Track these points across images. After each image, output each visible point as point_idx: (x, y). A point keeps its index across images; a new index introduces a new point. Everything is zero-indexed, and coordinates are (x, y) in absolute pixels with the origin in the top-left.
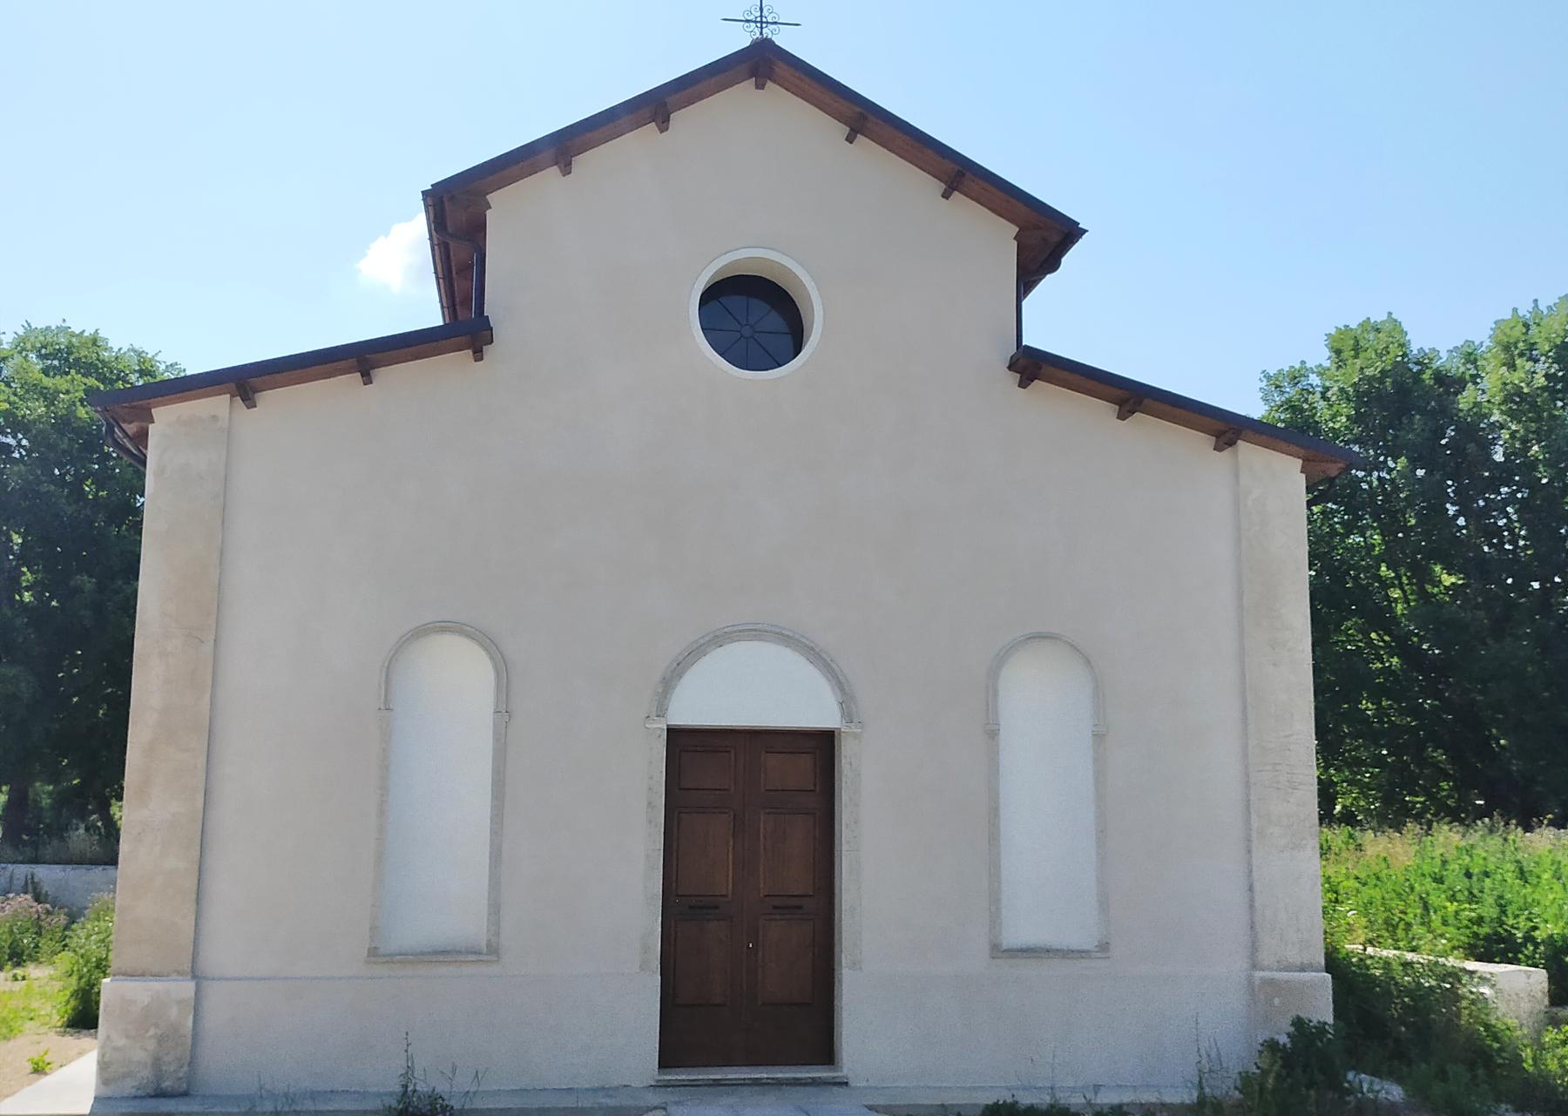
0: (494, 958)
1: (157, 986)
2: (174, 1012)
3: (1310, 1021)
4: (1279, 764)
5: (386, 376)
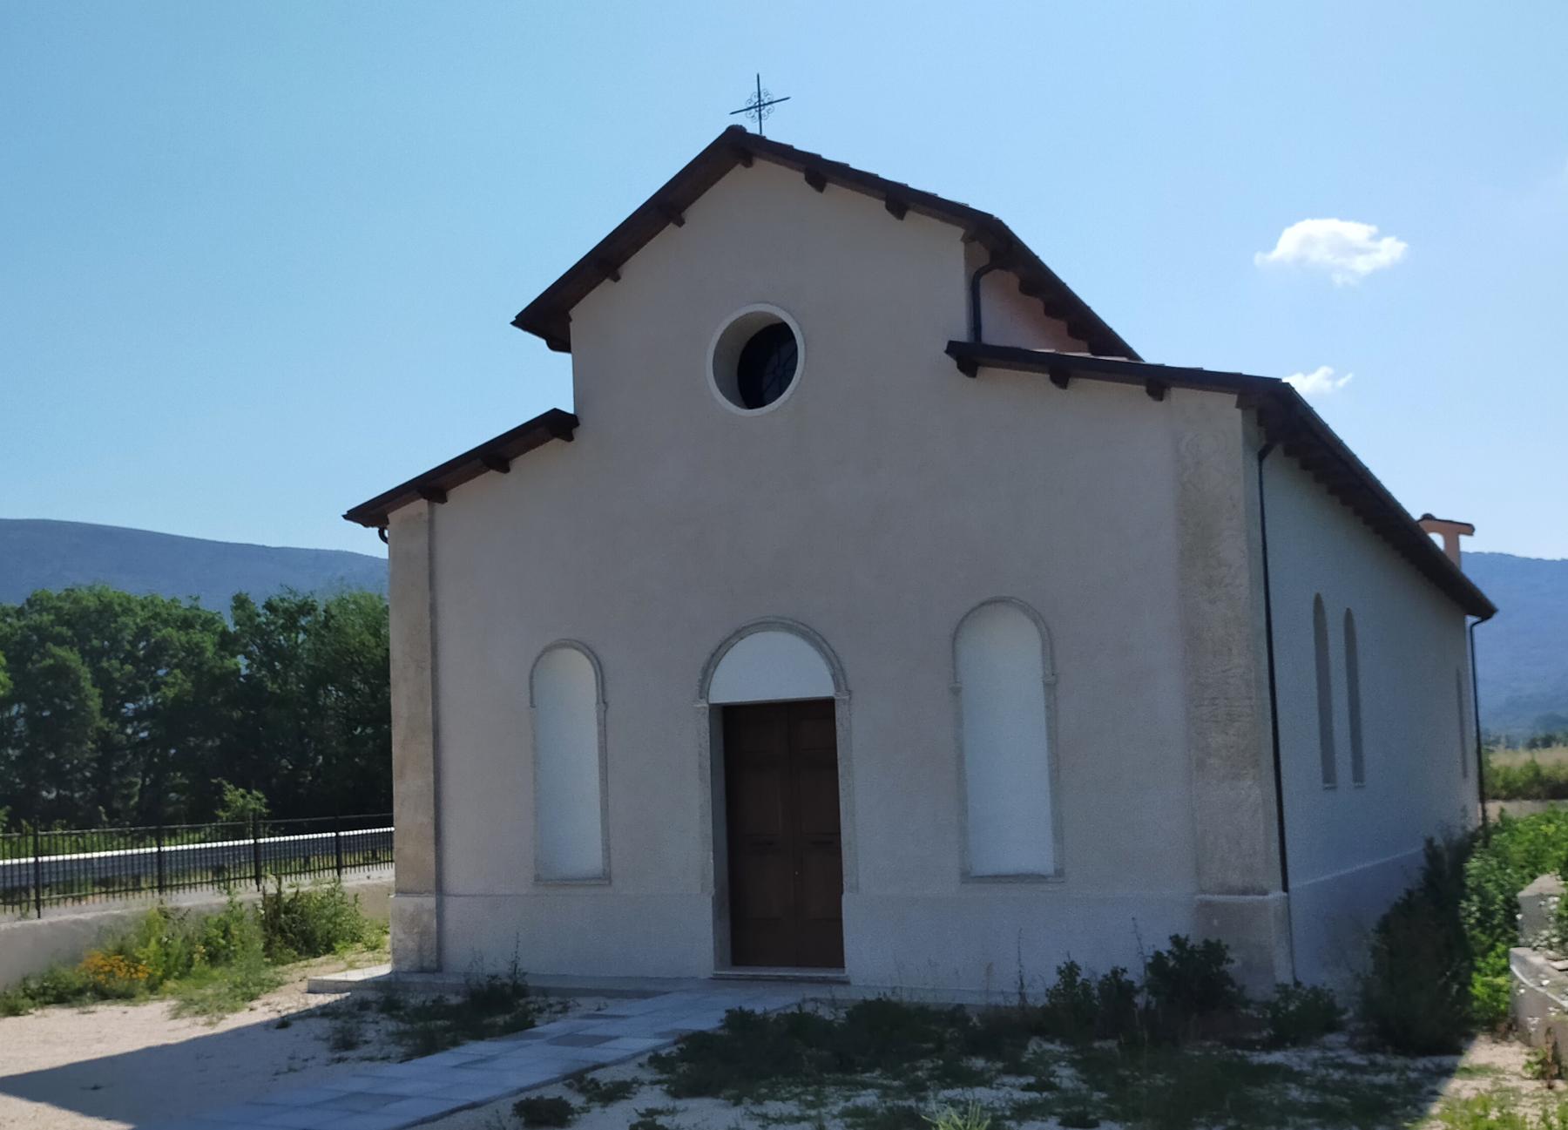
0: (607, 882)
1: (417, 900)
2: (425, 917)
3: (339, 1008)
4: (1216, 698)
5: (521, 464)
